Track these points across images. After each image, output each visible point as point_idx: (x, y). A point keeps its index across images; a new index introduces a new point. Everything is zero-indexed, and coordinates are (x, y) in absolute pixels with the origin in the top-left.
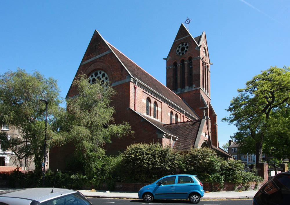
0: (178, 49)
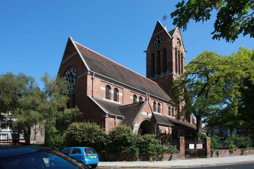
0: (155, 42)
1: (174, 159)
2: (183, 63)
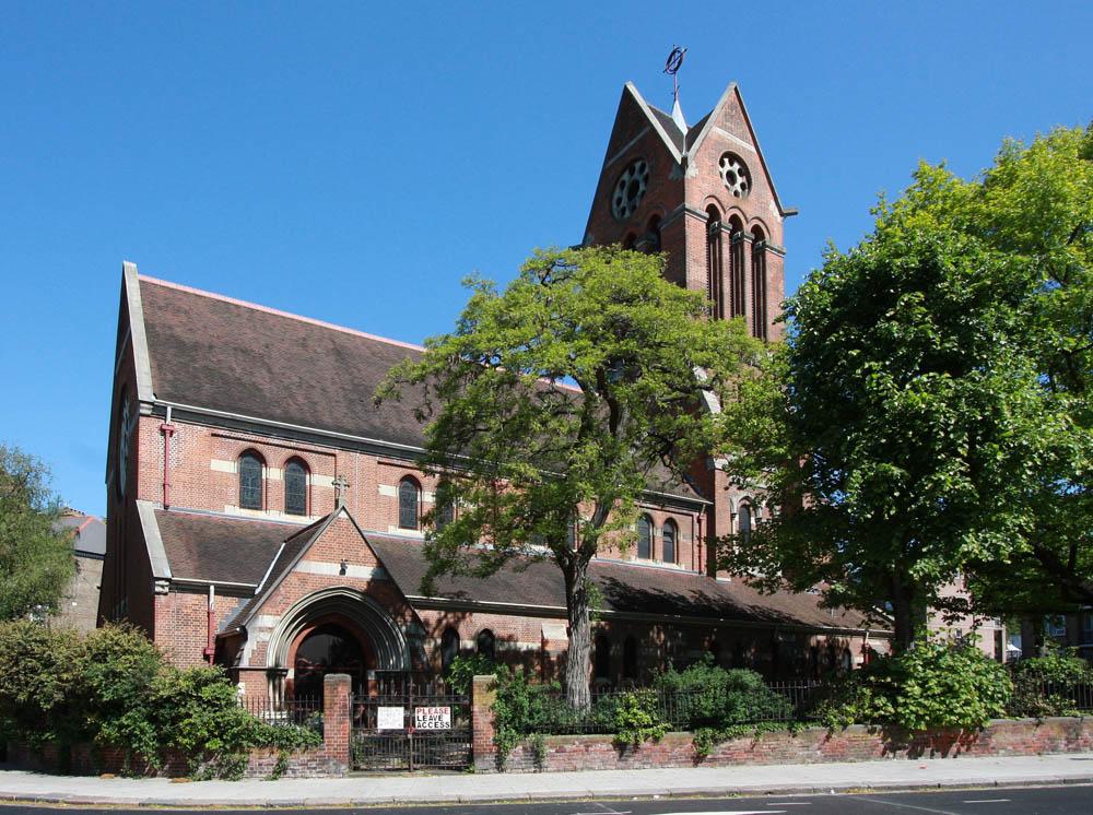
0: (617, 194)
1: (294, 771)
2: (770, 275)
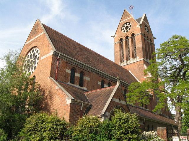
0: (123, 28)
